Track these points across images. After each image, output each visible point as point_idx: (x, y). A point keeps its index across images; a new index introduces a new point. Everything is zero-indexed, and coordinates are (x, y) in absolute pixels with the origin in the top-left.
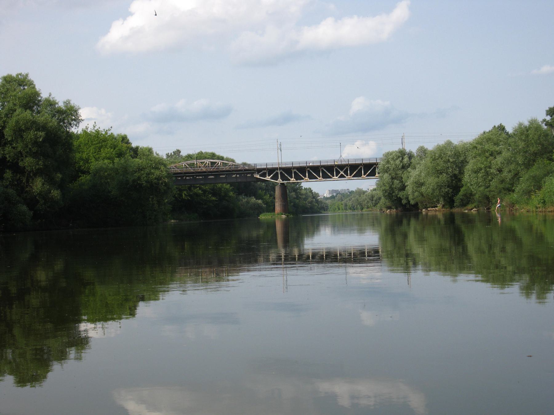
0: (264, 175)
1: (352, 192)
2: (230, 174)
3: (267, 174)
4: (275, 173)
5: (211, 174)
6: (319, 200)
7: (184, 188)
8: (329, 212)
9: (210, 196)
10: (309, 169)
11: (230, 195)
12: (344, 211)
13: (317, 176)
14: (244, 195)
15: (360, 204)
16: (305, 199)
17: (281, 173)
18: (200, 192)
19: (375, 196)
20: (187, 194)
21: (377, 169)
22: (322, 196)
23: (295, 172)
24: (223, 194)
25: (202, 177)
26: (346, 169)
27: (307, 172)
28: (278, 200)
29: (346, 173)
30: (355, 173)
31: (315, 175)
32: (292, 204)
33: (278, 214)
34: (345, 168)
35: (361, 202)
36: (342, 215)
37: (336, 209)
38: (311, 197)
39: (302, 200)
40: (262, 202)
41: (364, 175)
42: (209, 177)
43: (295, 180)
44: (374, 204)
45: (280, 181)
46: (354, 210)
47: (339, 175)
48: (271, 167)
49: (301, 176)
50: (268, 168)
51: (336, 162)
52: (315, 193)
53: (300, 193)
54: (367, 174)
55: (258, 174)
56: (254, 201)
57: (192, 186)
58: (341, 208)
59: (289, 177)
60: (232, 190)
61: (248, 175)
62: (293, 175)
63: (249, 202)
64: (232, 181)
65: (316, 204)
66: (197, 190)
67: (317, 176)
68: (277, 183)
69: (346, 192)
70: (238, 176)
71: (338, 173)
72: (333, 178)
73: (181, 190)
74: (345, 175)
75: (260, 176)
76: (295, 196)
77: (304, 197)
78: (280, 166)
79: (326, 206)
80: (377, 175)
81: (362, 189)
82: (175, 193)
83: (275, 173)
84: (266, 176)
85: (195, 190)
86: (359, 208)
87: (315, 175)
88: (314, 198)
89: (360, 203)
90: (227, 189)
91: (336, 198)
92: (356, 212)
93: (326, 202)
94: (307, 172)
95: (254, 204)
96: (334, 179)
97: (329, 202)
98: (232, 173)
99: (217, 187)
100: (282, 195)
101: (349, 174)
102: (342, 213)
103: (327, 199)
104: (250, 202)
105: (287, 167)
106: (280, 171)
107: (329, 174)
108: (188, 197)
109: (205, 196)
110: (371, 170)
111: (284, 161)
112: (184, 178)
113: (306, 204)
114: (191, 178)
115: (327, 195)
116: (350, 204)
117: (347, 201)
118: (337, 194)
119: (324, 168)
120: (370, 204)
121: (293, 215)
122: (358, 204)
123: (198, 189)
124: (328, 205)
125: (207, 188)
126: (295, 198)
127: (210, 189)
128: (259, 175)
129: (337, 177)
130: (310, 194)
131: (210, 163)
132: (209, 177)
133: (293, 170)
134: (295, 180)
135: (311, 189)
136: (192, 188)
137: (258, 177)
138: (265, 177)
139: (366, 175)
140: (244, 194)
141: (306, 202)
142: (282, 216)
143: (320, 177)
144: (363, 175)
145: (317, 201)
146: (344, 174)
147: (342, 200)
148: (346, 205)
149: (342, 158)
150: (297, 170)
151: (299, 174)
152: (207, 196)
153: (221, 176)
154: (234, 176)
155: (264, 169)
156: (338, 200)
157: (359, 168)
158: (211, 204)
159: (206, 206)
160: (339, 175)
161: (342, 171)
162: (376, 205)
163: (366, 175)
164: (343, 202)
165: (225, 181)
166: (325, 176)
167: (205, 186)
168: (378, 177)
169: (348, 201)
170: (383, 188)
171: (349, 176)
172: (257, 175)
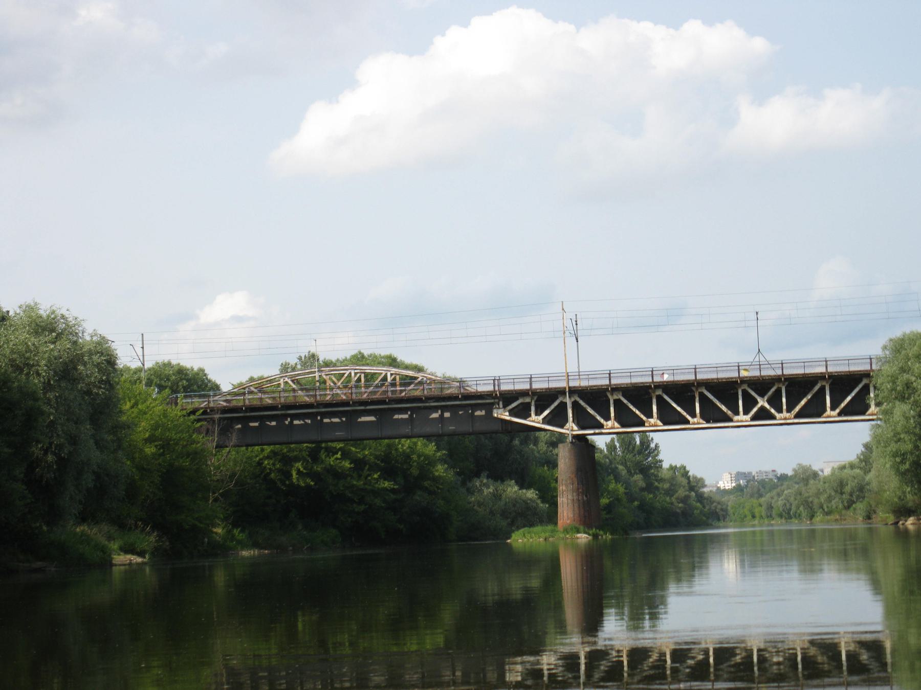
0: (523, 412)
1: (783, 478)
2: (419, 408)
3: (533, 408)
4: (556, 404)
5: (362, 408)
6: (706, 495)
7: (295, 453)
8: (731, 524)
9: (376, 476)
10: (659, 392)
11: (437, 474)
12: (766, 521)
13: (684, 414)
14: (488, 477)
15: (808, 505)
16: (670, 492)
17: (575, 405)
18: (347, 464)
19: (849, 482)
20: (305, 471)
21: (872, 389)
22: (713, 487)
23: (618, 403)
24: (415, 472)
25: (340, 419)
26: (776, 391)
27: (654, 401)
28: (567, 486)
29: (775, 402)
30: (803, 402)
31: (679, 409)
32: (636, 503)
33: (566, 531)
34: (773, 390)
35: (811, 499)
36: (761, 532)
37: (745, 516)
38: (684, 487)
39: (660, 494)
40: (536, 494)
41: (833, 408)
42: (359, 420)
43: (616, 425)
44: (846, 504)
45: (571, 428)
46: (791, 518)
47: (755, 410)
48: (544, 385)
49: (635, 413)
50: (537, 389)
51: (745, 370)
52: (695, 477)
53: (656, 476)
54: (843, 405)
55: (504, 407)
56: (516, 492)
57: (322, 448)
58: (757, 515)
59: (598, 418)
60: (443, 461)
61: (478, 413)
62: (612, 409)
63: (501, 495)
64: (428, 430)
65: (698, 504)
66: (337, 459)
67: (684, 414)
68: (562, 438)
69: (771, 476)
70: (447, 415)
71: (750, 403)
72: (736, 418)
73: (288, 461)
74: (773, 411)
75: (510, 415)
76: (642, 484)
77: (666, 486)
78: (573, 384)
79: (722, 510)
80: (873, 409)
81: (810, 466)
82: (270, 469)
83: (556, 404)
84: (530, 416)
85: (331, 461)
86: (804, 514)
87: (679, 409)
88: (692, 488)
89: (806, 502)
90: (427, 457)
91: (745, 490)
92: (794, 526)
93: (723, 499)
94: (654, 401)
95: (515, 502)
96: (738, 421)
97: (730, 501)
98: (427, 404)
99: (397, 449)
100: (577, 474)
101: (785, 407)
102: (761, 525)
103: (725, 492)
104: (504, 496)
105: (592, 386)
106: (573, 400)
107: (724, 408)
108: (308, 480)
109: (360, 476)
110: (853, 394)
111: (588, 366)
112: (287, 422)
113: (672, 504)
114: (307, 421)
115: (726, 483)
116: (779, 503)
117: (772, 498)
118: (748, 482)
119: (706, 389)
120: (836, 503)
121: (612, 534)
122: (802, 504)
123: (339, 456)
124: (727, 506)
125: (367, 453)
126: (642, 489)
127: (377, 457)
128: (510, 411)
129: (748, 417)
130: (684, 481)
131: (363, 376)
132: (359, 420)
133: (612, 395)
134: (619, 426)
135: (685, 468)
136: (323, 455)
137: (506, 416)
138: (527, 416)
139: (838, 411)
140: (485, 474)
141: (672, 498)
142: (579, 535)
143: (693, 415)
144: (828, 409)
145: (700, 498)
146: (768, 406)
147: (761, 496)
148: (770, 507)
149: (762, 359)
150: (624, 396)
151: (631, 407)
152: (369, 475)
153: (396, 417)
154: (435, 415)
155: (524, 393)
156: (752, 496)
157: (816, 388)
158: (378, 502)
159: (362, 507)
160: (755, 410)
161: (762, 396)
162: (852, 505)
163: (838, 411)
164: (762, 500)
165: (407, 430)
166: (713, 416)
167: (364, 449)
168: (875, 415)
169: (776, 498)
170: (893, 447)
171: (785, 414)
172: (501, 411)
